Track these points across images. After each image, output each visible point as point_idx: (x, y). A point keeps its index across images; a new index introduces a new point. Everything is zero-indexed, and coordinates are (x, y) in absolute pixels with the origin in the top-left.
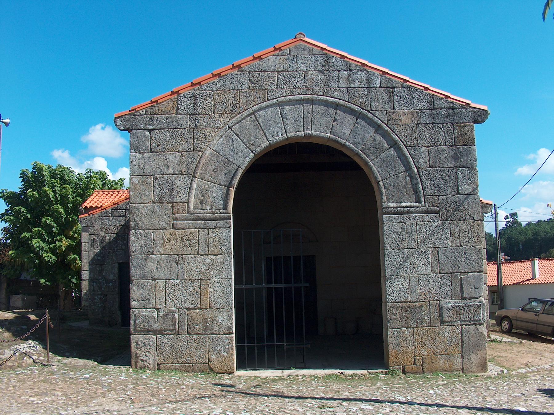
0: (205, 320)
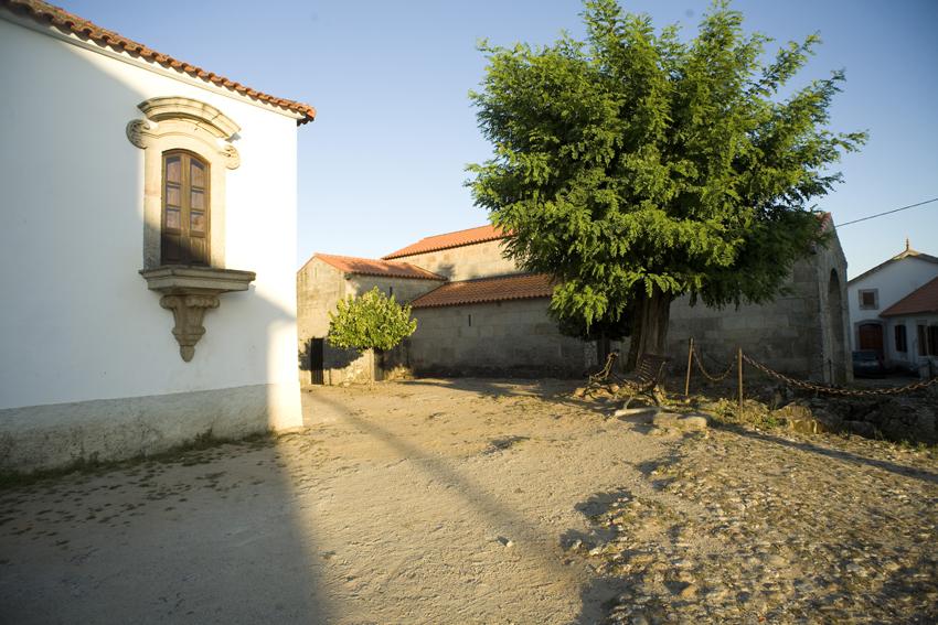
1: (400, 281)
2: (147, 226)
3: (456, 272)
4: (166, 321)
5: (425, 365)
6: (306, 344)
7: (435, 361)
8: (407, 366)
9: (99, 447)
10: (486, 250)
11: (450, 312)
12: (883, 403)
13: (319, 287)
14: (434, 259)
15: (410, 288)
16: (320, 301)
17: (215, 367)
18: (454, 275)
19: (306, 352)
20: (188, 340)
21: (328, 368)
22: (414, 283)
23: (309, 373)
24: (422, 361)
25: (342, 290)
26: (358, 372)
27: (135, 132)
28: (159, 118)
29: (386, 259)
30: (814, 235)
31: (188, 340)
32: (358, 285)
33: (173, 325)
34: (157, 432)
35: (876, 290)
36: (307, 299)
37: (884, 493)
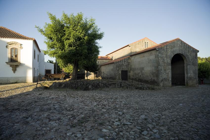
0: (168, 79)
1: (101, 60)
2: (9, 58)
4: (11, 68)
9: (2, 82)
10: (116, 53)
11: (107, 66)
15: (103, 61)
17: (19, 73)
20: (14, 70)
22: (104, 60)
26: (90, 77)
27: (7, 47)
28: (10, 44)
29: (106, 56)
30: (96, 50)
31: (14, 70)
33: (12, 69)
34: (9, 81)
35: (45, 69)
37: (33, 119)
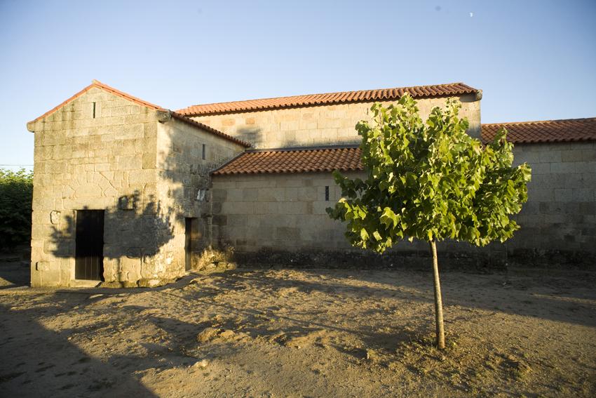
3: (264, 137)
5: (248, 248)
6: (68, 218)
7: (268, 244)
8: (220, 247)
12: (41, 262)
13: (100, 132)
14: (232, 123)
15: (219, 149)
16: (104, 153)
18: (260, 142)
19: (68, 230)
21: (116, 255)
23: (72, 261)
24: (245, 242)
25: (149, 137)
26: (169, 261)
32: (172, 132)
36: (74, 149)
